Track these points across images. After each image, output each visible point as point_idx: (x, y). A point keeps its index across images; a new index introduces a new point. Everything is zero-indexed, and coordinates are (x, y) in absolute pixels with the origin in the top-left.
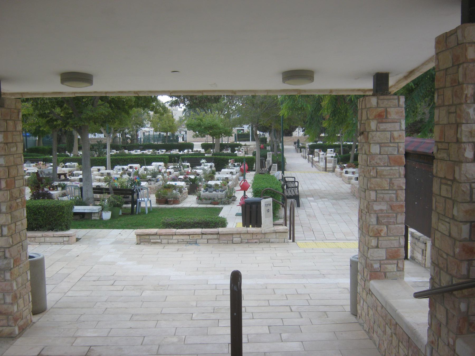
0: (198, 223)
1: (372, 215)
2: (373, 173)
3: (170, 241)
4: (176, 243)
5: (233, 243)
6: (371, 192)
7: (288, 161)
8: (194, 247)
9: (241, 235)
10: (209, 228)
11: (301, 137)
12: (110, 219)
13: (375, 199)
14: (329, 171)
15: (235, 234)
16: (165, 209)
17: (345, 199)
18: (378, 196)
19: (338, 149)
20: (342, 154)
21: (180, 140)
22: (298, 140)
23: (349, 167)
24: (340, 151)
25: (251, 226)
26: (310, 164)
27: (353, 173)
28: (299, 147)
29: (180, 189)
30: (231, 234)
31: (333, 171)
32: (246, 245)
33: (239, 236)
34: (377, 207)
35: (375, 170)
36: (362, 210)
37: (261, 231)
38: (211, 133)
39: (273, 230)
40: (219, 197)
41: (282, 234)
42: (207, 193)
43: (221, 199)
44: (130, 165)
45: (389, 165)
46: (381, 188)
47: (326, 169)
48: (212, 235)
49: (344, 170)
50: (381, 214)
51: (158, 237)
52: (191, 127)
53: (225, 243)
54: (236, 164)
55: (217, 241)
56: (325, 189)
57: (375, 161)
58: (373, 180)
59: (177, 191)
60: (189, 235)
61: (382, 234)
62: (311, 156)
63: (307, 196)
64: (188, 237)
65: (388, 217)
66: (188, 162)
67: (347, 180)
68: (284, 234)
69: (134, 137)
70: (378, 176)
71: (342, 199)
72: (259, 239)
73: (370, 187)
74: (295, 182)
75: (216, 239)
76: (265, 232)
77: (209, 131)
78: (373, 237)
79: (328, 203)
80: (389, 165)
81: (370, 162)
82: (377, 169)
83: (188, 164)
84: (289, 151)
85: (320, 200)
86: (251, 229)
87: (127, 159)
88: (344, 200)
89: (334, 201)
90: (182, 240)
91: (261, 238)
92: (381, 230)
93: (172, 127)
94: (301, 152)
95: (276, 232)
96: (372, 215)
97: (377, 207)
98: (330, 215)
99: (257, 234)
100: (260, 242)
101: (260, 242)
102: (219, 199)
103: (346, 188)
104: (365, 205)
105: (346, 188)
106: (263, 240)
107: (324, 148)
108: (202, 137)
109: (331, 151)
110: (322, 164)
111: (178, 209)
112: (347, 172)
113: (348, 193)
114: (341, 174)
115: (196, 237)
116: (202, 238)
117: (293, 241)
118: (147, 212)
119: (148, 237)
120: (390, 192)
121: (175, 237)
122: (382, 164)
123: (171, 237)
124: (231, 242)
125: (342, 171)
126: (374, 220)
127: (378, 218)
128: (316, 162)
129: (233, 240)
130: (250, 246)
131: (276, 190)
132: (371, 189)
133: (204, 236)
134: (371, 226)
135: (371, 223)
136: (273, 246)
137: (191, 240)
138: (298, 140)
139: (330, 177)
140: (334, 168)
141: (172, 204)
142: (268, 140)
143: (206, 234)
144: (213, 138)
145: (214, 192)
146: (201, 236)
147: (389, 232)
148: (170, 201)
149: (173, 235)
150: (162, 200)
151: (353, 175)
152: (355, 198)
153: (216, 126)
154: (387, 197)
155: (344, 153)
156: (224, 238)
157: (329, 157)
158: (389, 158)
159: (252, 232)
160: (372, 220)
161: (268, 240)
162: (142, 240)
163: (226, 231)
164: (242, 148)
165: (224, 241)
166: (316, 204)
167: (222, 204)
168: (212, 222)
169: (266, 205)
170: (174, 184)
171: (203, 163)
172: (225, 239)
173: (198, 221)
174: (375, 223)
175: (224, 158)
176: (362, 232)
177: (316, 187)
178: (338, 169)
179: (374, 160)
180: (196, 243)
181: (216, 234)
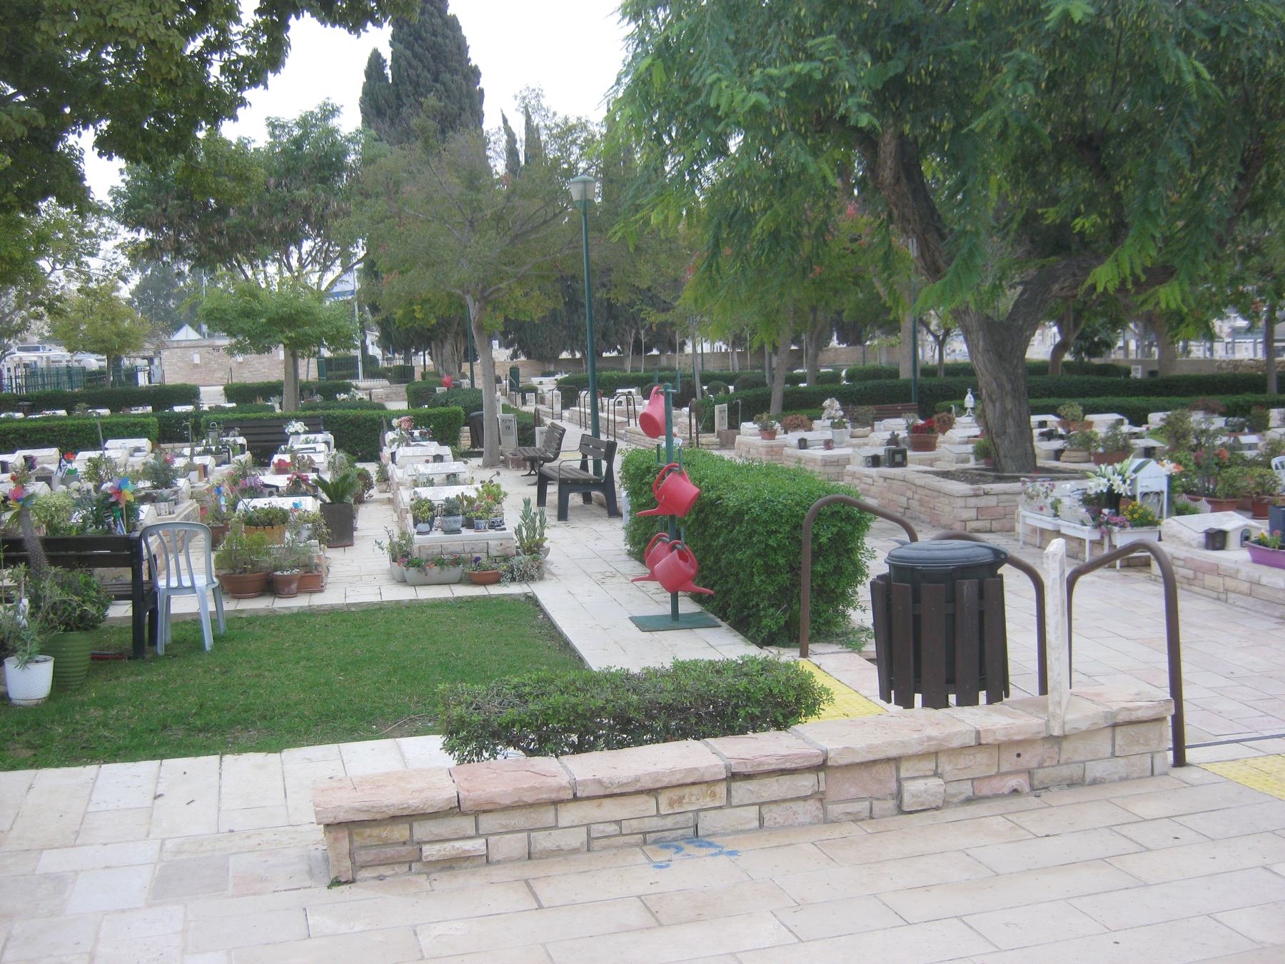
3: (544, 841)
4: (575, 851)
5: (900, 811)
9: (943, 759)
12: (51, 698)
21: (143, 380)
30: (888, 760)
33: (928, 766)
38: (290, 339)
40: (493, 553)
43: (506, 558)
51: (467, 824)
52: (222, 320)
53: (856, 819)
54: (416, 433)
64: (646, 805)
68: (1157, 725)
72: (1030, 773)
75: (805, 798)
83: (242, 440)
90: (613, 829)
91: (1040, 766)
93: (125, 335)
99: (1015, 746)
101: (1037, 789)
111: (312, 612)
115: (694, 800)
116: (729, 804)
118: (208, 641)
119: (400, 832)
121: (569, 815)
123: (548, 816)
124: (891, 804)
129: (899, 795)
137: (669, 822)
141: (291, 595)
143: (748, 777)
145: (467, 533)
148: (288, 581)
149: (556, 803)
150: (241, 577)
153: (307, 314)
159: (1001, 737)
161: (1074, 771)
162: (363, 856)
163: (870, 748)
167: (513, 580)
171: (297, 433)
172: (853, 791)
175: (357, 418)
180: (696, 837)
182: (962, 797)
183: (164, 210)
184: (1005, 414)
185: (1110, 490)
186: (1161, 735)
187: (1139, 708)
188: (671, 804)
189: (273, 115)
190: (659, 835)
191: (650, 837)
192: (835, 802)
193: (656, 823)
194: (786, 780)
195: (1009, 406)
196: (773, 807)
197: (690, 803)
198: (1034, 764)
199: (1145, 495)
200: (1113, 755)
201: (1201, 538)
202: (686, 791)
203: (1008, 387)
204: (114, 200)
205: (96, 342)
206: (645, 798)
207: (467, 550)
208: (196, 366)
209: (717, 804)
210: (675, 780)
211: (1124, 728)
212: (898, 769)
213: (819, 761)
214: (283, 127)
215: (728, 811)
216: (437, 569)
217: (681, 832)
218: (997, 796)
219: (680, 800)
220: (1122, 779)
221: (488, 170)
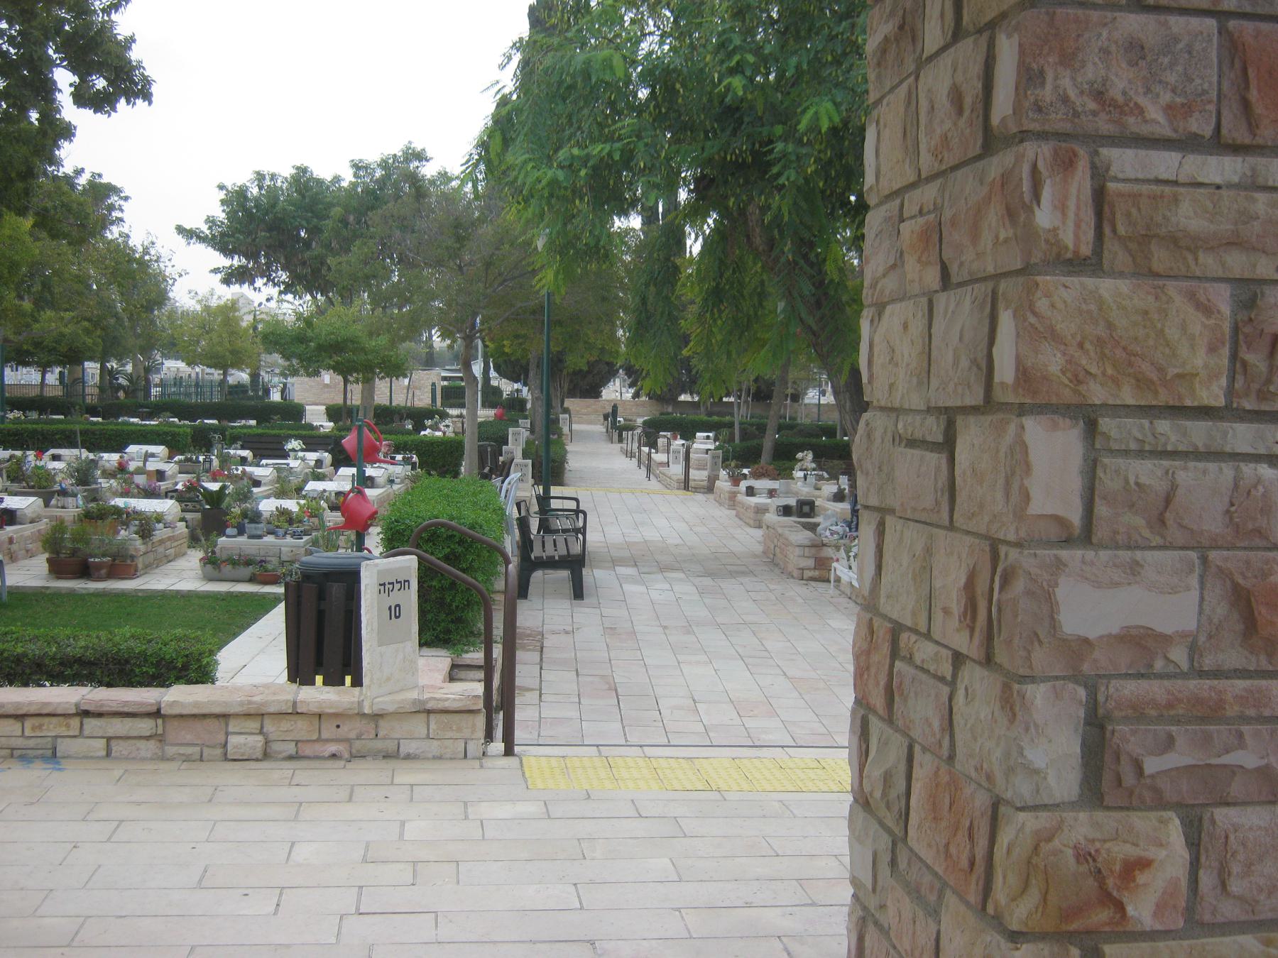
0: (80, 661)
1: (1038, 694)
2: (1059, 215)
5: (226, 758)
6: (1034, 428)
7: (575, 462)
8: (36, 773)
10: (130, 684)
11: (624, 402)
13: (1075, 516)
14: (697, 490)
15: (237, 715)
16: (72, 594)
17: (743, 573)
18: (1108, 482)
19: (725, 431)
20: (737, 440)
21: (276, 397)
22: (615, 408)
23: (757, 476)
24: (732, 434)
25: (319, 679)
26: (643, 471)
27: (772, 493)
28: (616, 427)
29: (146, 526)
31: (710, 489)
32: (279, 771)
33: (254, 725)
34: (1093, 605)
35: (1081, 182)
36: (896, 629)
37: (360, 703)
38: (337, 362)
39: (415, 702)
40: (284, 558)
41: (457, 717)
42: (243, 539)
44: (52, 451)
45: (1234, 130)
46: (1142, 383)
47: (686, 484)
48: (128, 721)
49: (744, 484)
50: (1130, 688)
53: (187, 759)
54: (399, 457)
55: (152, 745)
56: (679, 541)
57: (1090, 73)
58: (1063, 295)
59: (133, 529)
60: (21, 717)
61: (1141, 910)
62: (646, 449)
63: (615, 562)
65: (1209, 712)
66: (243, 448)
67: (752, 515)
68: (470, 717)
69: (140, 384)
70: (1115, 253)
71: (733, 574)
72: (347, 740)
73: (1024, 375)
74: (577, 511)
76: (376, 709)
77: (331, 357)
78: (1042, 936)
79: (684, 588)
80: (1234, 130)
81: (1029, 77)
82: (1100, 176)
84: (586, 437)
85: (660, 576)
86: (318, 694)
87: (54, 434)
88: (742, 579)
89: (707, 581)
92: (1133, 868)
93: (238, 352)
94: (621, 440)
95: (429, 712)
96: (1038, 694)
97: (1093, 605)
98: (688, 630)
99: (339, 717)
100: (353, 757)
102: (282, 563)
103: (748, 539)
104: (950, 579)
105: (748, 539)
106: (369, 743)
107: (687, 432)
108: (309, 375)
109: (708, 437)
110: (677, 470)
112: (751, 491)
113: (755, 556)
114: (733, 496)
115: (52, 728)
116: (81, 734)
117: (509, 751)
120: (1241, 436)
122: (1156, 119)
124: (219, 751)
125: (735, 489)
126: (1054, 753)
127: (1096, 730)
128: (661, 464)
130: (301, 776)
131: (472, 527)
132: (1035, 398)
133: (90, 724)
134: (1018, 830)
135: (1022, 788)
136: (406, 775)
137: (31, 743)
138: (615, 408)
139: (697, 505)
140: (713, 479)
142: (529, 406)
143: (100, 715)
144: (346, 381)
146: (75, 722)
147: (1207, 880)
148: (99, 566)
150: (70, 559)
151: (769, 501)
152: (777, 571)
154: (1203, 490)
155: (743, 439)
156: (187, 734)
157: (698, 451)
158: (1233, 49)
159: (314, 709)
160: (1037, 756)
161: (391, 746)
163: (196, 704)
164: (447, 422)
165: (183, 750)
166: (642, 589)
168: (144, 656)
169: (385, 587)
170: (122, 505)
171: (293, 450)
172: (189, 738)
173: (78, 652)
174: (1064, 781)
176: (898, 841)
177: (651, 534)
178: (723, 483)
179: (1068, 59)
181: (149, 715)
182: (285, 754)
183: (254, 240)
186: (474, 725)
187: (447, 699)
188: (33, 729)
189: (357, 157)
190: (24, 752)
191: (17, 753)
192: (173, 745)
193: (19, 742)
194: (128, 722)
196: (120, 741)
197: (48, 729)
198: (353, 735)
200: (428, 737)
202: (46, 720)
204: (210, 228)
205: (211, 358)
206: (11, 721)
207: (262, 553)
208: (327, 386)
209: (71, 733)
210: (33, 710)
211: (438, 716)
212: (227, 725)
213: (154, 709)
214: (366, 168)
215: (80, 740)
216: (229, 567)
217: (40, 752)
218: (317, 758)
219: (40, 727)
220: (434, 758)
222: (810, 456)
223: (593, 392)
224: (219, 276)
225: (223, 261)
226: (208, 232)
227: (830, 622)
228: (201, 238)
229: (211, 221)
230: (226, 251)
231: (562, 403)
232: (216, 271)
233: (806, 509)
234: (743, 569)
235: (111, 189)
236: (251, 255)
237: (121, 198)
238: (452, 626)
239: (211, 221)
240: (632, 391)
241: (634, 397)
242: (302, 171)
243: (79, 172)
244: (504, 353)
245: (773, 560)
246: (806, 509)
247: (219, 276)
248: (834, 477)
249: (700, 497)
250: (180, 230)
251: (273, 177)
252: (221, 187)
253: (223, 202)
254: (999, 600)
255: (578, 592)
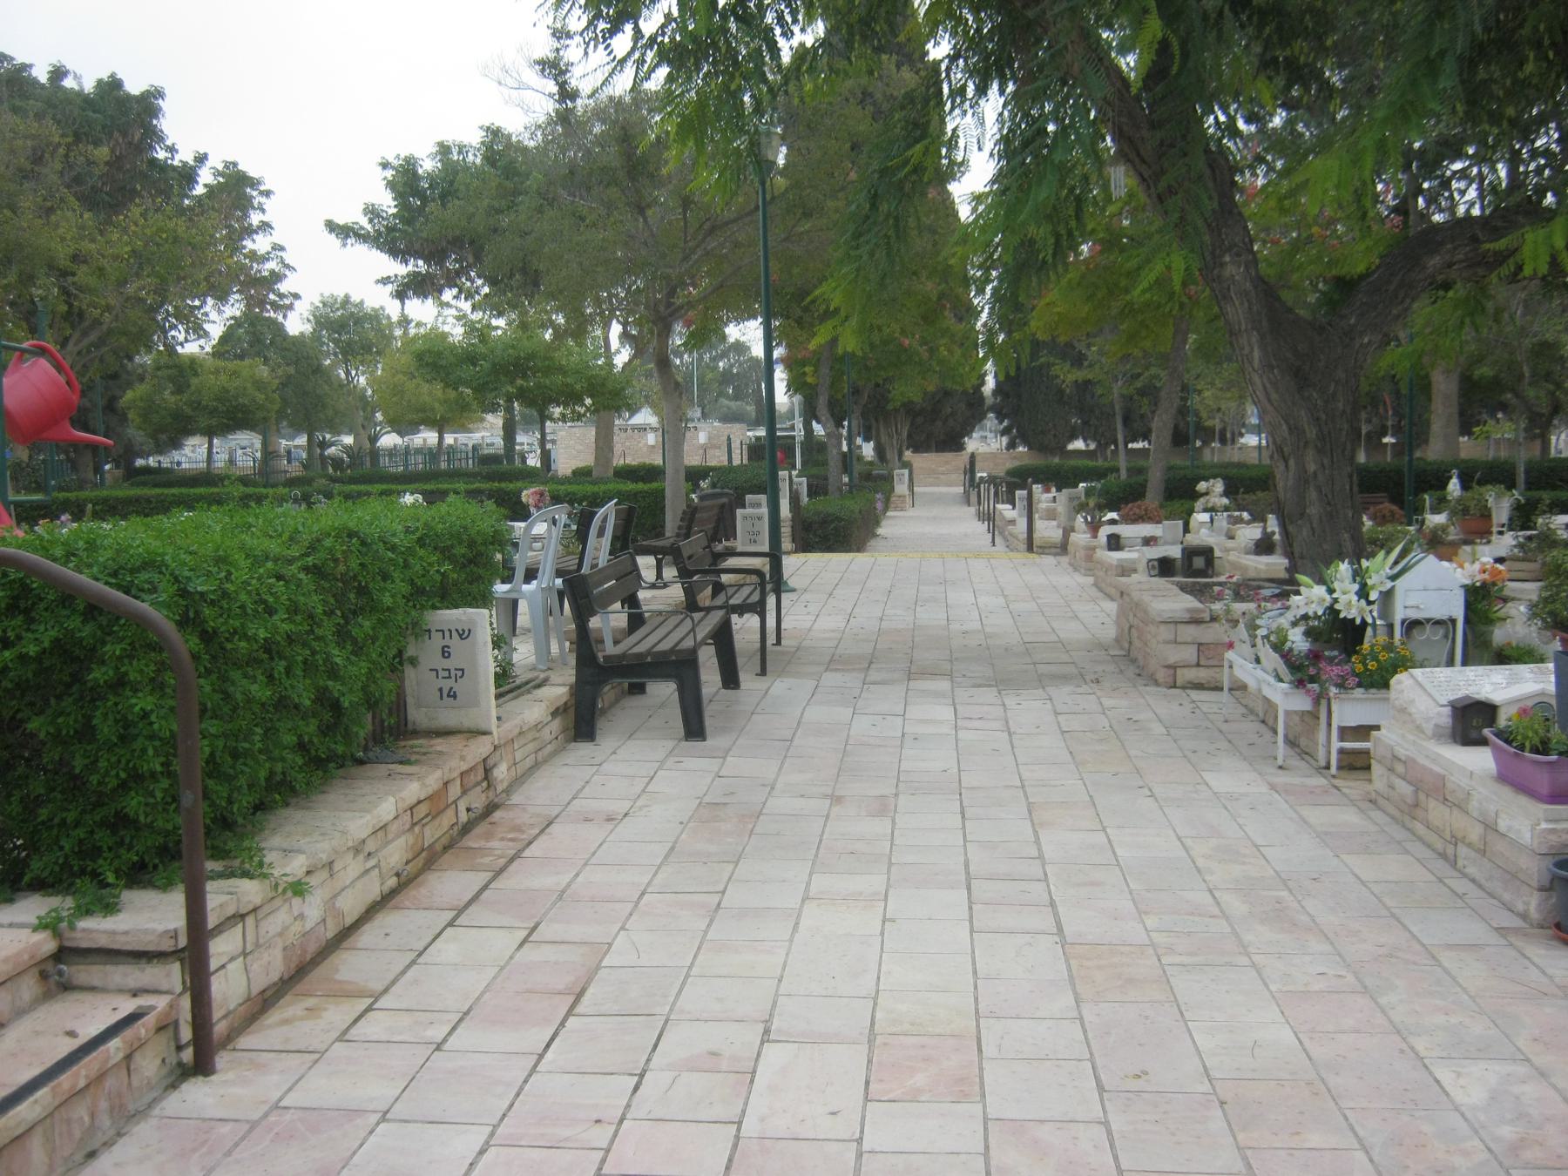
17: (1064, 679)
31: (1063, 548)
105: (1097, 617)
112: (1115, 543)
152: (1131, 671)
178: (1081, 537)
184: (1304, 480)
185: (1332, 611)
195: (1312, 467)
199: (1412, 625)
201: (1444, 717)
203: (1311, 433)
204: (371, 221)
221: (955, 214)
222: (1218, 486)
223: (953, 443)
224: (390, 288)
225: (400, 269)
226: (369, 227)
227: (1207, 776)
228: (362, 237)
229: (372, 212)
230: (394, 252)
231: (900, 454)
232: (385, 281)
233: (1199, 562)
234: (1072, 670)
235: (254, 183)
236: (434, 255)
237: (261, 193)
238: (103, 838)
239: (372, 212)
240: (1005, 440)
241: (1008, 448)
242: (495, 133)
243: (201, 159)
244: (805, 383)
245: (1130, 658)
246: (1199, 562)
247: (390, 288)
248: (1258, 517)
249: (1049, 560)
250: (331, 226)
251: (462, 149)
252: (385, 165)
253: (391, 185)
254: (368, 494)
255: (694, 728)
